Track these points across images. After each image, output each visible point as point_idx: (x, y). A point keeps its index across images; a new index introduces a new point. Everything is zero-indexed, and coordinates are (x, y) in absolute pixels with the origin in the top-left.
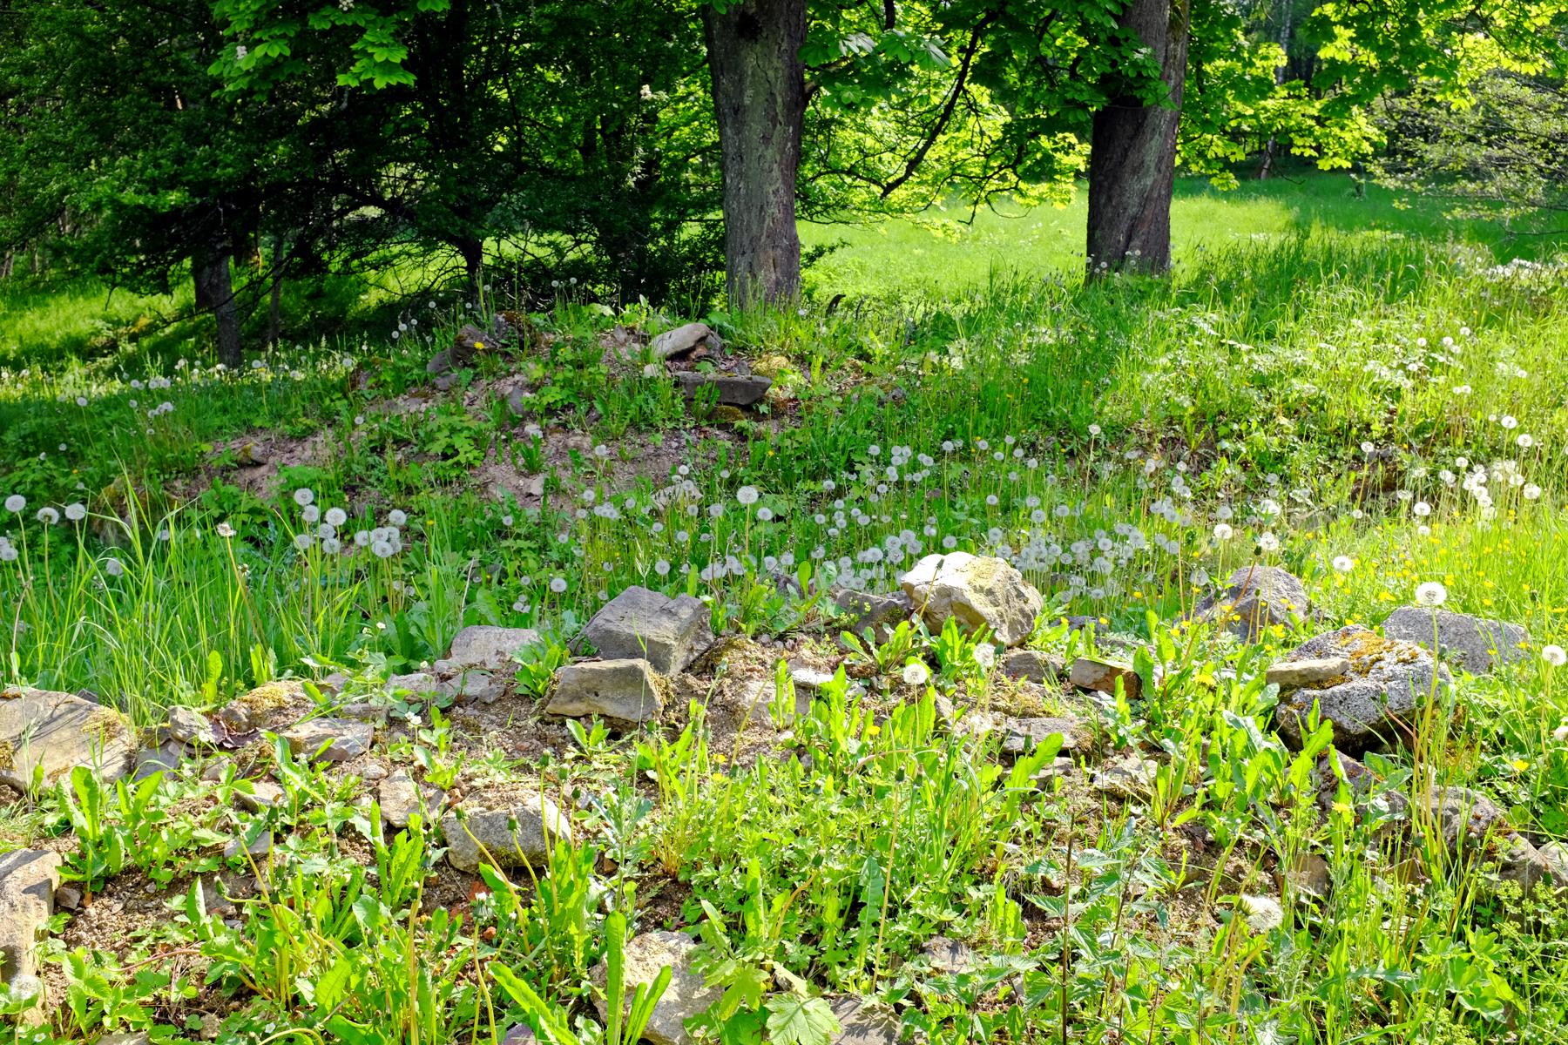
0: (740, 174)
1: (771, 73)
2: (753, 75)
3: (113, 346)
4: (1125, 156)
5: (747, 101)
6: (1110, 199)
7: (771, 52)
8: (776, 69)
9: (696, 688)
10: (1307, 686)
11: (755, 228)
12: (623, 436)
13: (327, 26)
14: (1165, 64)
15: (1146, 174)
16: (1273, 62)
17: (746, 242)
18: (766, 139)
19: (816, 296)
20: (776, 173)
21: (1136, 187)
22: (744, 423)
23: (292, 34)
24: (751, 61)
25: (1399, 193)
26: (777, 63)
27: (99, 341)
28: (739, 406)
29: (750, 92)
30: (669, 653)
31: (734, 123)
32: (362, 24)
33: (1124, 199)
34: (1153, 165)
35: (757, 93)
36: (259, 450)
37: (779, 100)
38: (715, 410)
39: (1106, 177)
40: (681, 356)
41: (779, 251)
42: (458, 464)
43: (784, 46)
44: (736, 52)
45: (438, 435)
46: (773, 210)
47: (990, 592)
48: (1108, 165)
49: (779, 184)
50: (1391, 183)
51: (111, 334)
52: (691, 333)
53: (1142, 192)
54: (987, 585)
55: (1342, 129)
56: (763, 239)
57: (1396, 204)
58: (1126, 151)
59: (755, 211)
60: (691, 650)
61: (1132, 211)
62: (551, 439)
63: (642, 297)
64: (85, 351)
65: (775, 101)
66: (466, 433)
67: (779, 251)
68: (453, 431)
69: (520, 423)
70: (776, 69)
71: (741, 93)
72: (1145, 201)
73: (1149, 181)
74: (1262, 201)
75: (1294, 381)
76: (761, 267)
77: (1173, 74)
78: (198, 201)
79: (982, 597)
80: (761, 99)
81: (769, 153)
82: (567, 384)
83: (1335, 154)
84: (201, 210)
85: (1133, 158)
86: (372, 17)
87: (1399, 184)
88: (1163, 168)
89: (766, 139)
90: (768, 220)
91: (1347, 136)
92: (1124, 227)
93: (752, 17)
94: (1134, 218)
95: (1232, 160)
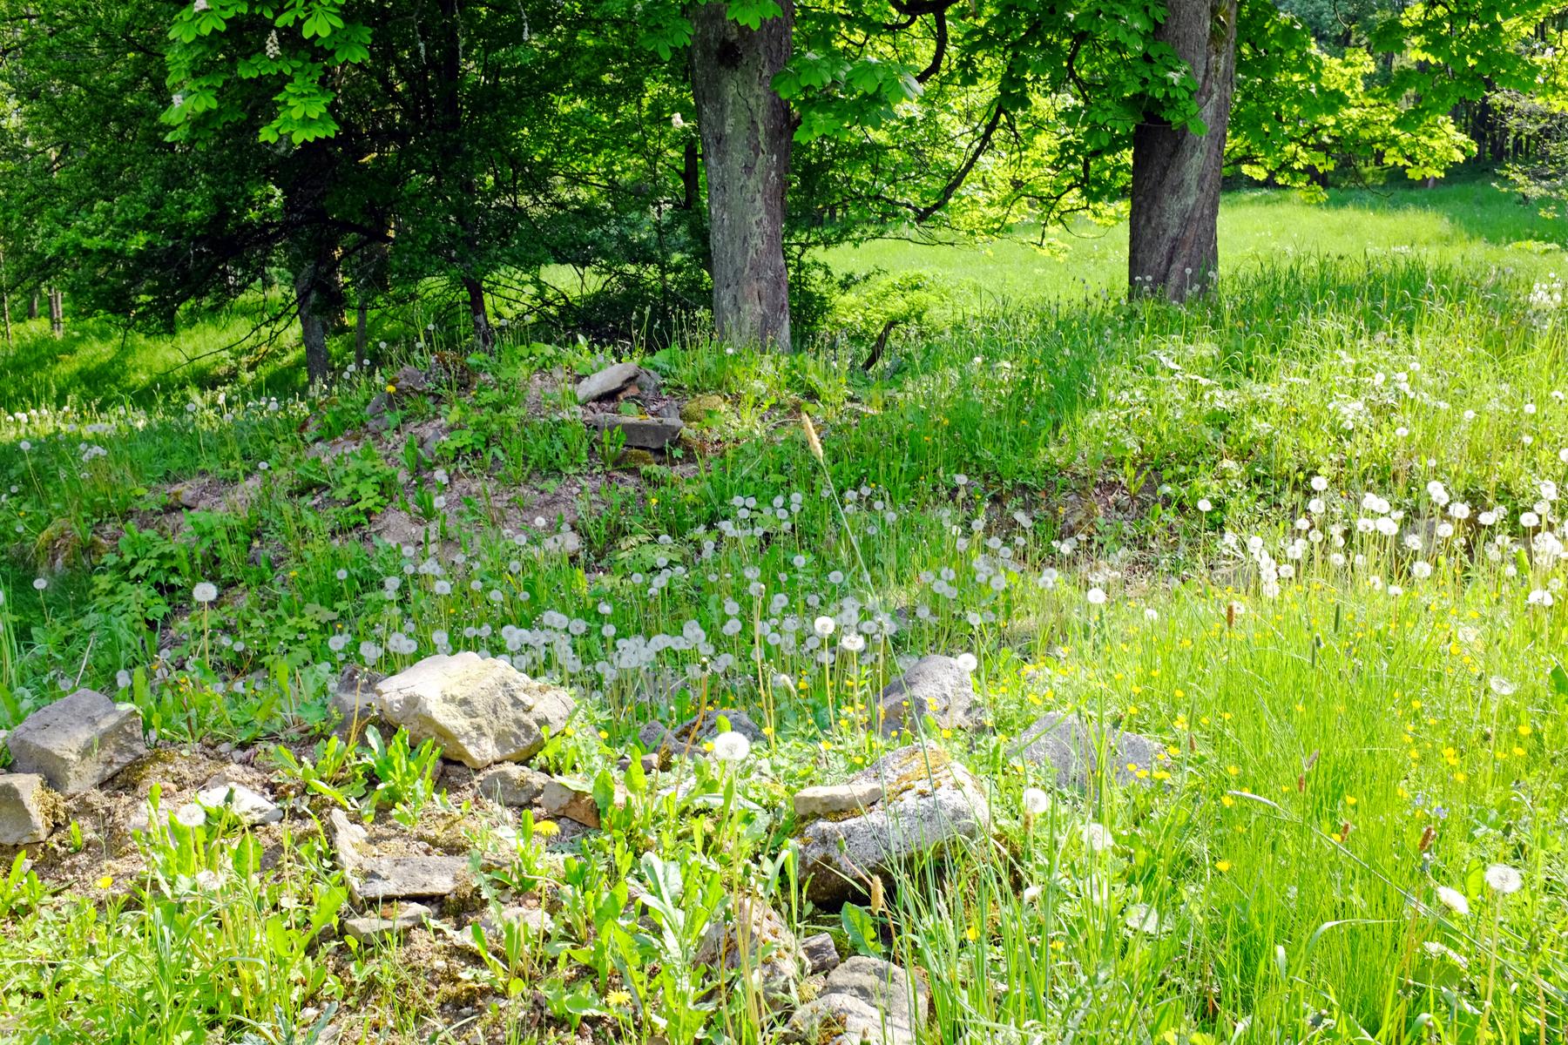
0: (723, 205)
1: (752, 101)
2: (734, 103)
3: (233, 375)
4: (1164, 175)
5: (728, 130)
6: (1149, 220)
7: (752, 79)
8: (758, 97)
9: (96, 805)
10: (825, 817)
11: (738, 259)
12: (526, 483)
13: (255, 75)
14: (1205, 77)
15: (1187, 194)
16: (1361, 69)
17: (730, 275)
18: (748, 169)
19: (925, 317)
20: (759, 203)
21: (1174, 209)
22: (654, 468)
23: (220, 84)
24: (732, 90)
25: (1544, 201)
26: (758, 91)
27: (222, 370)
28: (651, 450)
29: (731, 121)
30: (67, 768)
31: (717, 153)
32: (288, 72)
33: (1164, 220)
34: (1194, 184)
35: (738, 122)
36: (190, 493)
37: (761, 128)
38: (625, 454)
39: (1146, 198)
40: (610, 396)
41: (764, 283)
42: (358, 511)
43: (766, 73)
44: (718, 81)
45: (345, 480)
46: (756, 241)
47: (465, 702)
48: (1148, 185)
49: (762, 214)
50: (1535, 191)
51: (233, 363)
52: (620, 372)
53: (1183, 212)
54: (460, 693)
55: (1431, 137)
56: (747, 271)
57: (1542, 213)
58: (1165, 169)
59: (738, 243)
60: (109, 763)
61: (1173, 232)
62: (457, 485)
63: (581, 338)
64: (207, 381)
65: (757, 130)
66: (374, 479)
67: (764, 283)
68: (362, 477)
69: (431, 468)
70: (758, 97)
71: (723, 123)
72: (1187, 220)
73: (1191, 201)
74: (1431, 214)
75: (1254, 420)
76: (745, 301)
77: (1215, 87)
78: (170, 243)
79: (453, 708)
80: (743, 127)
81: (751, 183)
82: (479, 427)
83: (1426, 164)
84: (173, 254)
85: (1172, 175)
86: (298, 64)
87: (1543, 191)
88: (1206, 186)
89: (748, 169)
90: (751, 252)
91: (1435, 143)
92: (1165, 249)
93: (733, 44)
94: (1175, 239)
95: (1321, 170)
